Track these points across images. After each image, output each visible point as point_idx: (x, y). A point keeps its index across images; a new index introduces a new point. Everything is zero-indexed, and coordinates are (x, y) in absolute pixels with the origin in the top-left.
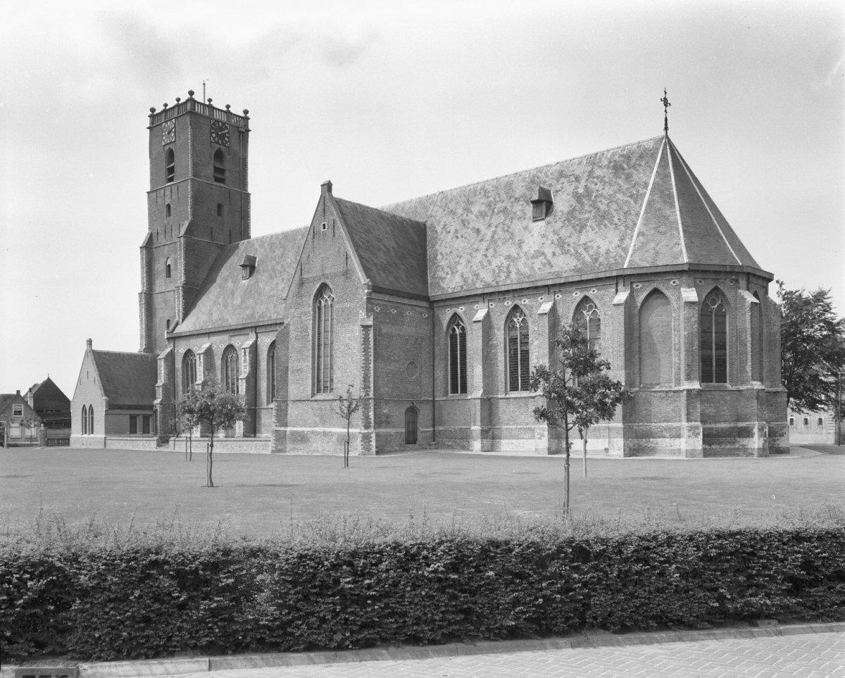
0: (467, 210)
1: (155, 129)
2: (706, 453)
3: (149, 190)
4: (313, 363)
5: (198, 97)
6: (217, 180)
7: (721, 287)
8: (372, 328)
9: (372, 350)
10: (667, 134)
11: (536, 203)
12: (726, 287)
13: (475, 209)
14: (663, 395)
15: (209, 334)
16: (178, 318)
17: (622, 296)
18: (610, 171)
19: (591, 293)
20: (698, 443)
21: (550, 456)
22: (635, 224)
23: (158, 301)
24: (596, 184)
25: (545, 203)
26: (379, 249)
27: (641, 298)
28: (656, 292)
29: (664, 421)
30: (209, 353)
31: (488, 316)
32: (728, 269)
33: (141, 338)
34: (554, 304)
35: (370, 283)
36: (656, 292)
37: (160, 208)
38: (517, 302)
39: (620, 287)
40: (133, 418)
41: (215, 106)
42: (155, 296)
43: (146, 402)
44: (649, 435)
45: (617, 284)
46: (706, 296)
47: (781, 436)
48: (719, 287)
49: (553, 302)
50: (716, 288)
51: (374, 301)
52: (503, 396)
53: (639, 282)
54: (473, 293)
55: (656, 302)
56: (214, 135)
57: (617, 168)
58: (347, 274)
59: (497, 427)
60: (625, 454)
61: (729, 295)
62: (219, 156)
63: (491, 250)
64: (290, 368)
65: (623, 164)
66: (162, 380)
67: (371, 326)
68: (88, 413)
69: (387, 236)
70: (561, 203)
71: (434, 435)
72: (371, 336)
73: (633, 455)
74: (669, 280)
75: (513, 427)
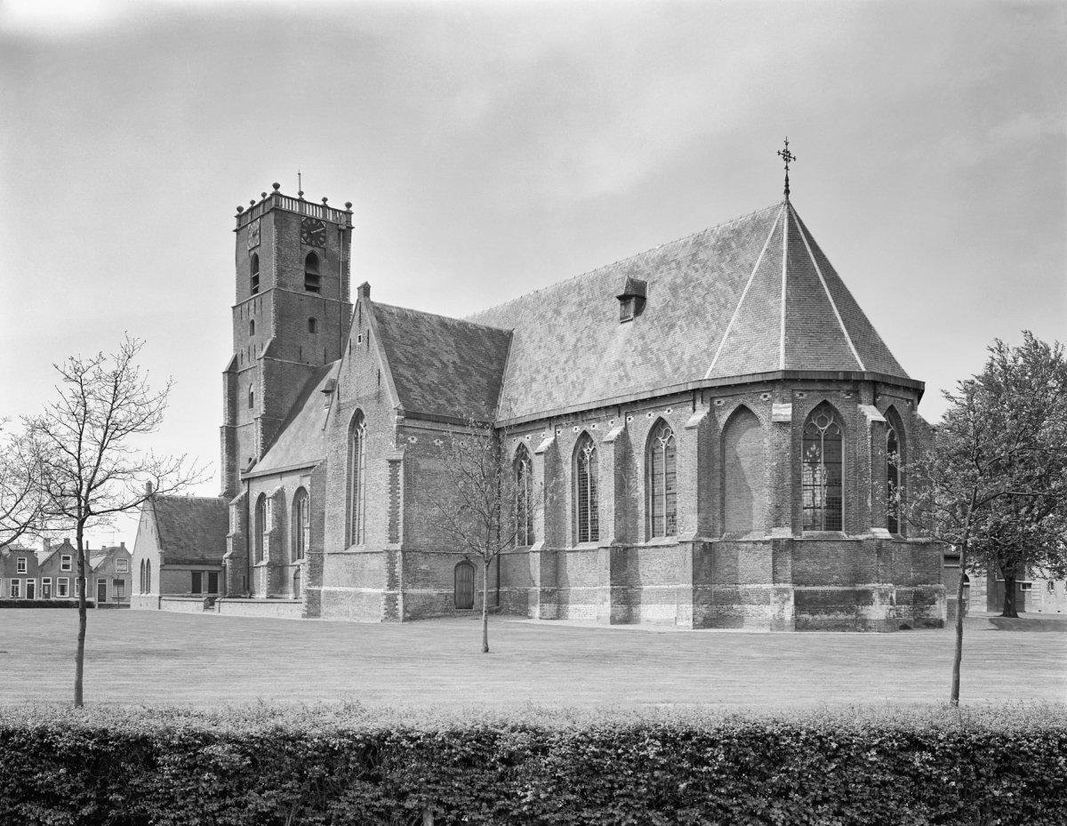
0: (557, 312)
1: (241, 232)
2: (800, 626)
3: (235, 304)
4: (348, 507)
5: (289, 190)
6: (309, 288)
7: (832, 401)
8: (402, 463)
9: (401, 491)
10: (787, 198)
11: (624, 299)
12: (840, 401)
13: (565, 311)
14: (750, 546)
15: (281, 474)
16: (257, 454)
17: (701, 413)
18: (716, 252)
19: (665, 414)
20: (789, 611)
21: (614, 627)
22: (728, 322)
23: (241, 433)
24: (697, 271)
25: (634, 299)
26: (431, 365)
27: (723, 420)
28: (742, 409)
29: (751, 582)
30: (279, 496)
31: (555, 445)
32: (841, 377)
33: (222, 481)
34: (626, 429)
35: (401, 408)
36: (742, 409)
37: (245, 323)
38: (586, 427)
39: (698, 404)
40: (196, 577)
41: (307, 201)
42: (238, 430)
43: (213, 556)
44: (736, 598)
45: (694, 401)
46: (810, 414)
47: (931, 604)
48: (830, 401)
49: (624, 426)
50: (825, 402)
51: (407, 429)
52: (570, 548)
53: (722, 397)
54: (537, 417)
55: (742, 423)
56: (305, 235)
57: (723, 246)
58: (379, 396)
59: (564, 588)
60: (694, 625)
61: (844, 411)
62: (312, 260)
63: (571, 363)
64: (326, 513)
65: (729, 243)
66: (234, 529)
67: (399, 461)
68: (145, 566)
69: (447, 349)
70: (653, 299)
71: (497, 598)
72: (401, 473)
73: (711, 626)
74: (760, 393)
75: (581, 588)
